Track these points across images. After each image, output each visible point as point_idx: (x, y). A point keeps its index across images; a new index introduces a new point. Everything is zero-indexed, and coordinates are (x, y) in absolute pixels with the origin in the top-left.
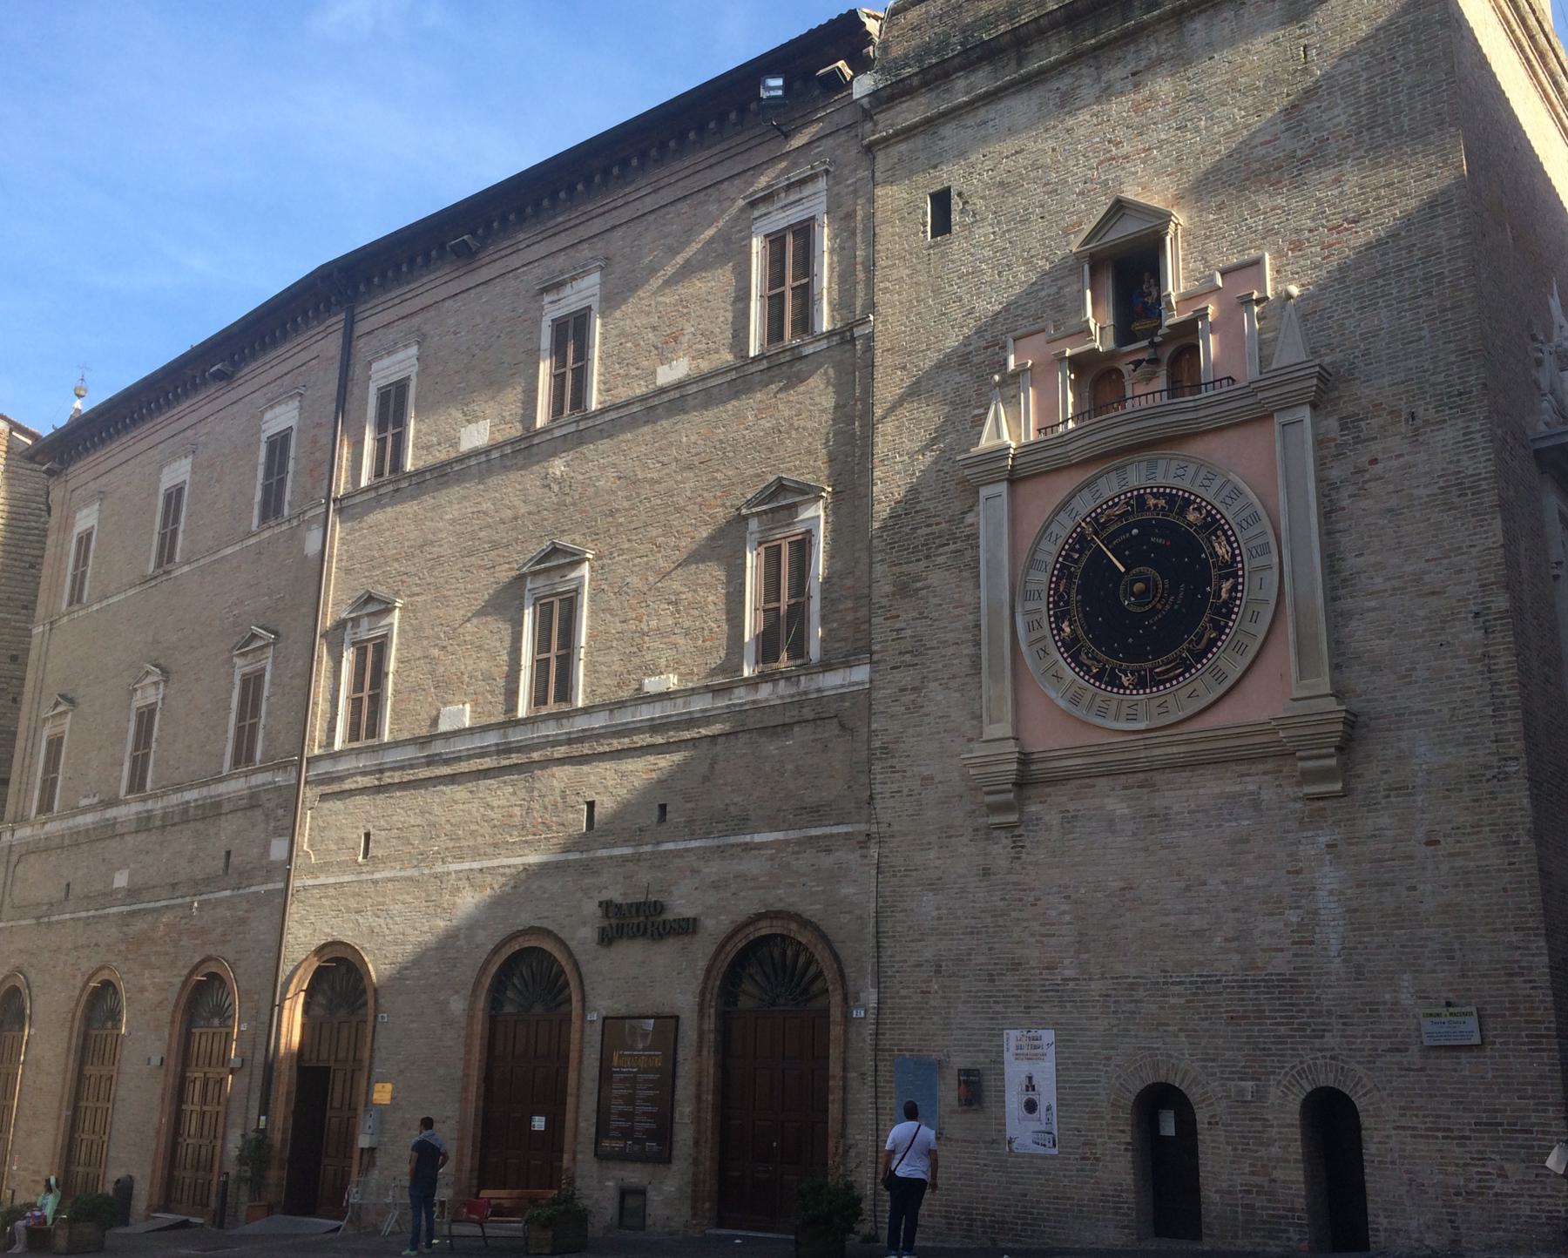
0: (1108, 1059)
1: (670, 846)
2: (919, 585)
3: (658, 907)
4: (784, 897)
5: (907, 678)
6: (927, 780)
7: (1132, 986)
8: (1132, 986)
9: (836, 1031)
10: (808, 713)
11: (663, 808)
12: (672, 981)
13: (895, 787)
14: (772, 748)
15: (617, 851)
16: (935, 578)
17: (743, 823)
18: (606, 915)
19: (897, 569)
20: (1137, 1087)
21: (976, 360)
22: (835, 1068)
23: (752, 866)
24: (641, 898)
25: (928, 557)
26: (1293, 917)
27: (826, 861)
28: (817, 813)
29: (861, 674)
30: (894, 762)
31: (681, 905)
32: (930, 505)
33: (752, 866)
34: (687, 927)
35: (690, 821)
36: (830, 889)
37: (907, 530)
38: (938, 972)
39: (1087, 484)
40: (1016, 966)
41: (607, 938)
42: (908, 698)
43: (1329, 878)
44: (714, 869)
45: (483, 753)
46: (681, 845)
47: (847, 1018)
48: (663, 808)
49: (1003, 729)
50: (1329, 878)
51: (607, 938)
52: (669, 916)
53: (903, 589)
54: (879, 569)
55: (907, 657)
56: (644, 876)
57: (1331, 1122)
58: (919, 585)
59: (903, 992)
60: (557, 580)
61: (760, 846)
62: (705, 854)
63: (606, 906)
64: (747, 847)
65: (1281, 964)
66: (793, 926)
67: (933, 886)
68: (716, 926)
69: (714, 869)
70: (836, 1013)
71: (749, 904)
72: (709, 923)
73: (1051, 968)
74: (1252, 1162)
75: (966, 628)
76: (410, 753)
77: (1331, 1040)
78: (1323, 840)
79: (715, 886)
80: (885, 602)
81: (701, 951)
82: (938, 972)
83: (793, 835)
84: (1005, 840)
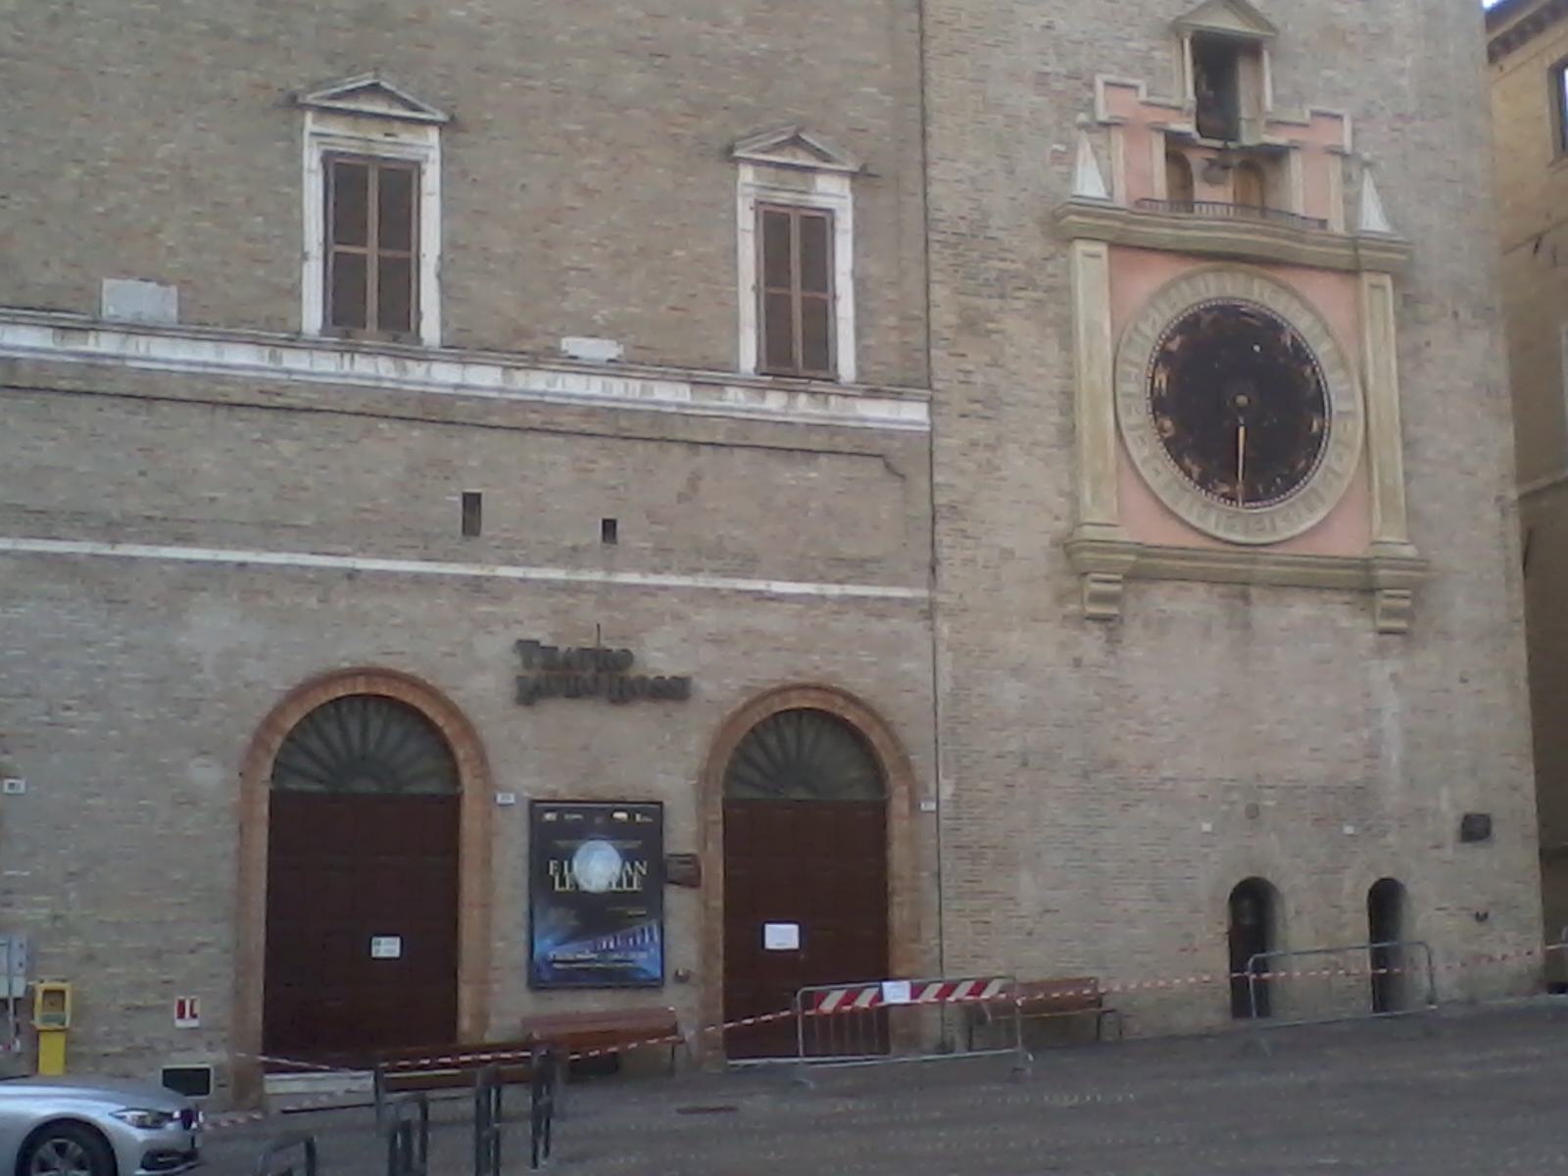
0: (1206, 855)
1: (634, 578)
2: (991, 326)
4: (816, 666)
5: (980, 431)
6: (1007, 554)
7: (1229, 789)
8: (1229, 789)
10: (840, 443)
11: (609, 528)
13: (968, 553)
15: (534, 574)
16: (1011, 324)
18: (527, 664)
19: (963, 299)
20: (1235, 881)
21: (1058, 86)
23: (769, 621)
24: (589, 643)
25: (1002, 296)
26: (1365, 734)
27: (879, 627)
29: (913, 413)
30: (962, 525)
31: (656, 658)
32: (1000, 234)
33: (769, 621)
34: (672, 691)
36: (887, 668)
37: (975, 255)
38: (1025, 764)
39: (1187, 278)
40: (1112, 764)
41: (530, 694)
42: (981, 455)
43: (1391, 704)
44: (709, 619)
45: (189, 331)
46: (653, 580)
47: (914, 806)
48: (609, 528)
49: (741, 132)
50: (1391, 704)
51: (530, 694)
52: (633, 673)
53: (972, 324)
54: (939, 293)
55: (977, 406)
56: (588, 613)
57: (1384, 902)
58: (991, 326)
59: (984, 785)
60: (380, 137)
61: (780, 598)
63: (527, 647)
64: (760, 597)
65: (1355, 775)
66: (840, 701)
67: (1017, 671)
68: (725, 684)
69: (709, 619)
72: (705, 688)
73: (1149, 767)
74: (1320, 937)
75: (1051, 393)
76: (19, 320)
77: (1391, 839)
78: (1388, 670)
79: (716, 640)
80: (947, 333)
82: (1025, 764)
83: (834, 590)
84: (1097, 631)
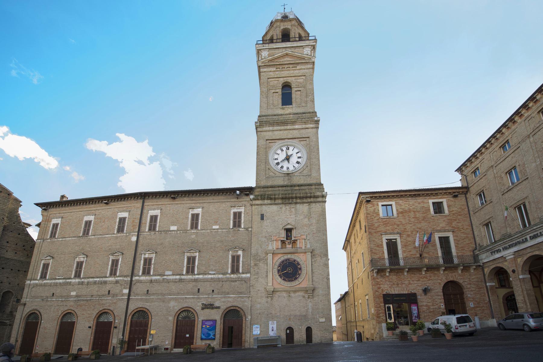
3: (213, 305)
4: (235, 304)
9: (244, 322)
11: (213, 291)
12: (217, 315)
14: (233, 284)
17: (228, 293)
22: (244, 326)
23: (230, 299)
27: (242, 300)
28: (241, 293)
31: (217, 304)
33: (230, 299)
34: (218, 308)
35: (218, 293)
41: (203, 309)
48: (213, 291)
51: (203, 309)
56: (210, 300)
62: (221, 298)
63: (203, 304)
64: (229, 297)
68: (223, 307)
69: (223, 300)
70: (244, 319)
71: (229, 305)
72: (222, 307)
81: (221, 311)
